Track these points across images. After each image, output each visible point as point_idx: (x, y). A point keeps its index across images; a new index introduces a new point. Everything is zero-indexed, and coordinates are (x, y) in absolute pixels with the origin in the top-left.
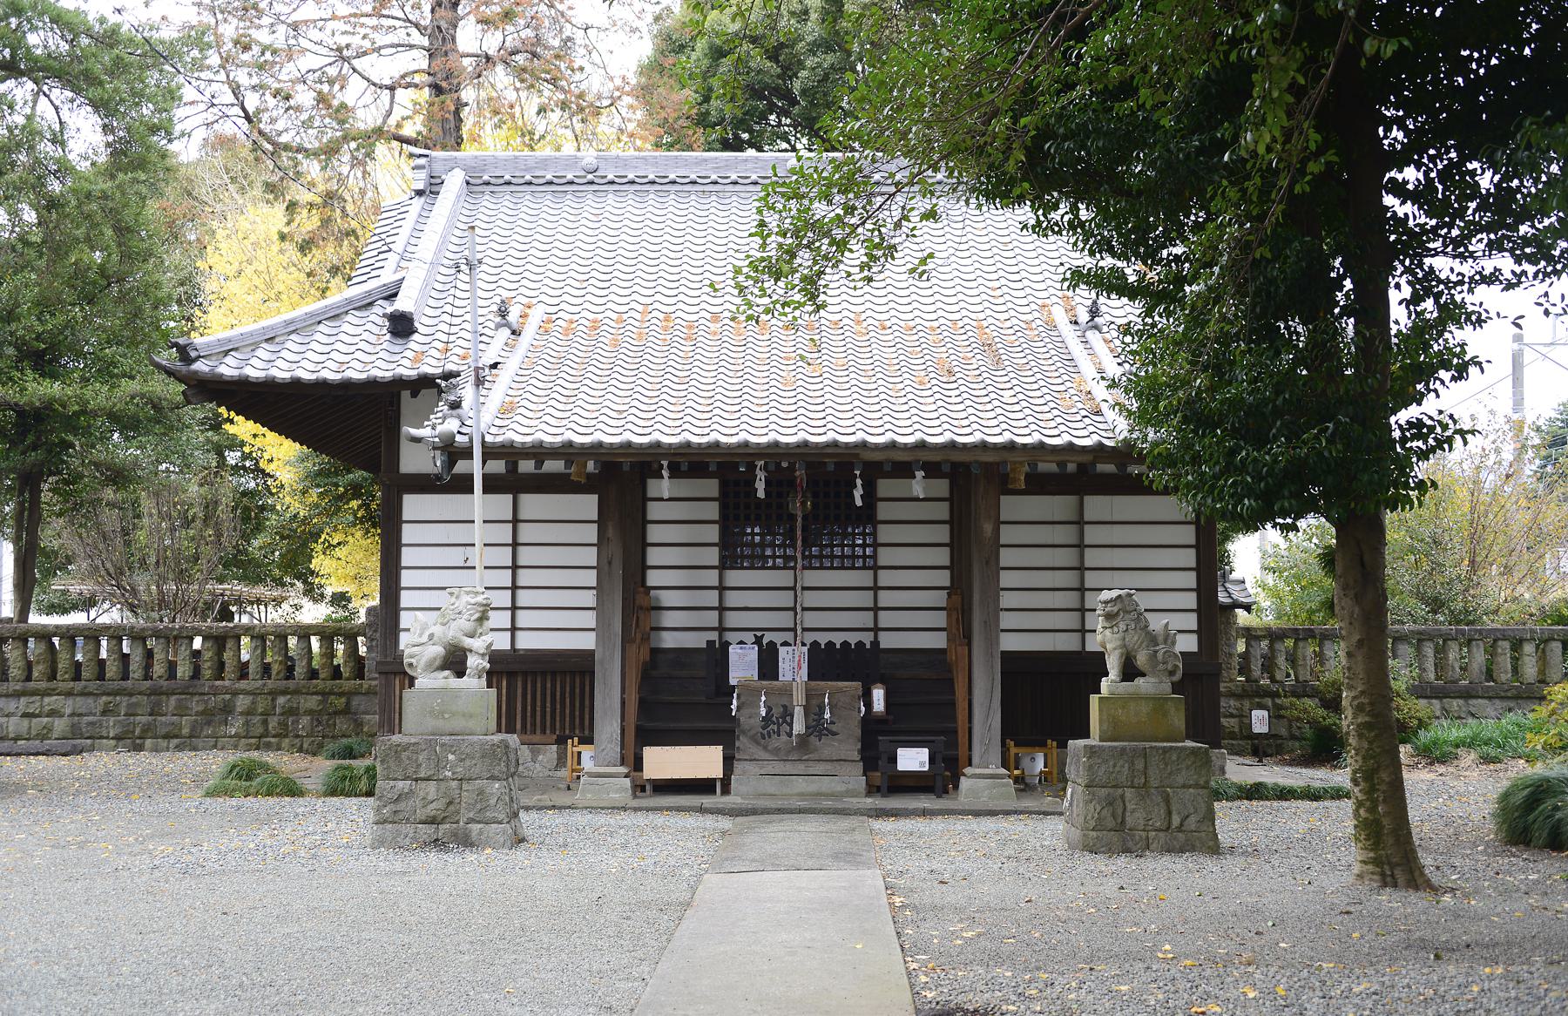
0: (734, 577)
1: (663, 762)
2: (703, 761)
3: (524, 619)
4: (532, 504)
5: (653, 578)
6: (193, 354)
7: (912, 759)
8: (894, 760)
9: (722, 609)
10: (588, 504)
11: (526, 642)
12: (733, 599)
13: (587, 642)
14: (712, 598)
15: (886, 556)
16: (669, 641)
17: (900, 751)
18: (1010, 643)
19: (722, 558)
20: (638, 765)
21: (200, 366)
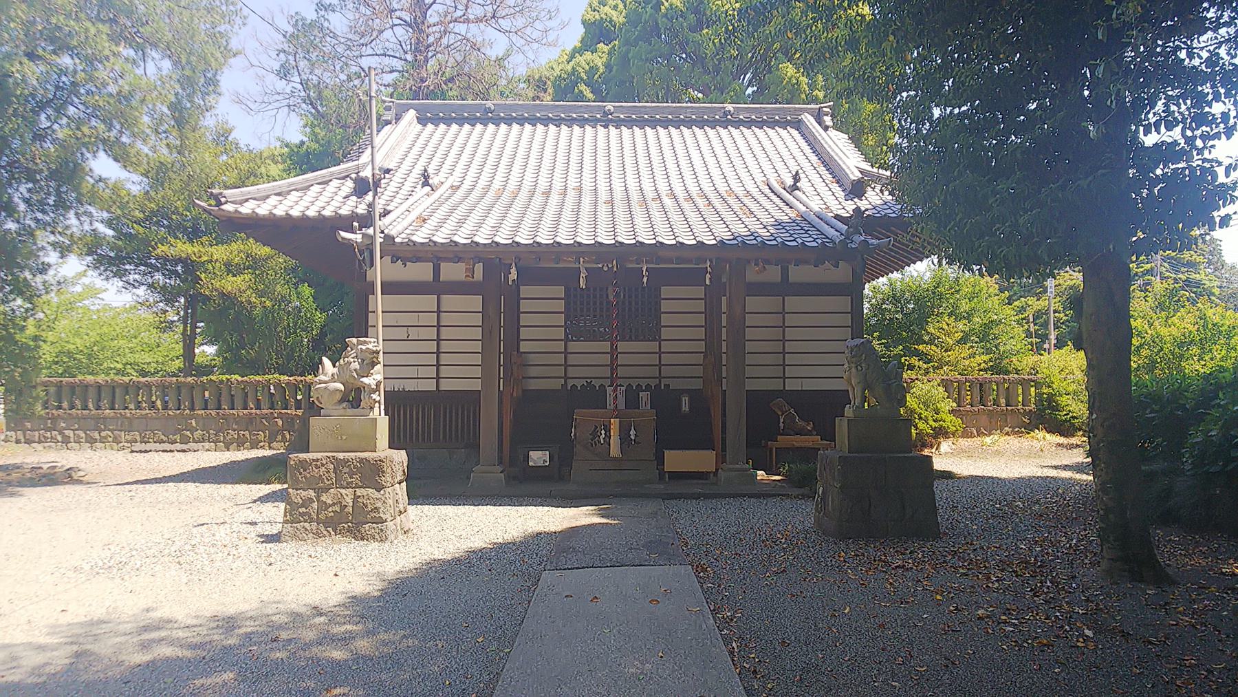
0: (574, 346)
1: (676, 460)
2: (702, 460)
3: (444, 371)
4: (449, 301)
5: (524, 347)
6: (223, 200)
7: (538, 457)
8: (527, 458)
9: (566, 366)
10: (476, 302)
11: (446, 386)
12: (572, 359)
13: (476, 386)
14: (789, 347)
15: (665, 334)
16: (534, 385)
17: (667, 453)
18: (751, 385)
19: (566, 335)
20: (660, 460)
21: (229, 207)
